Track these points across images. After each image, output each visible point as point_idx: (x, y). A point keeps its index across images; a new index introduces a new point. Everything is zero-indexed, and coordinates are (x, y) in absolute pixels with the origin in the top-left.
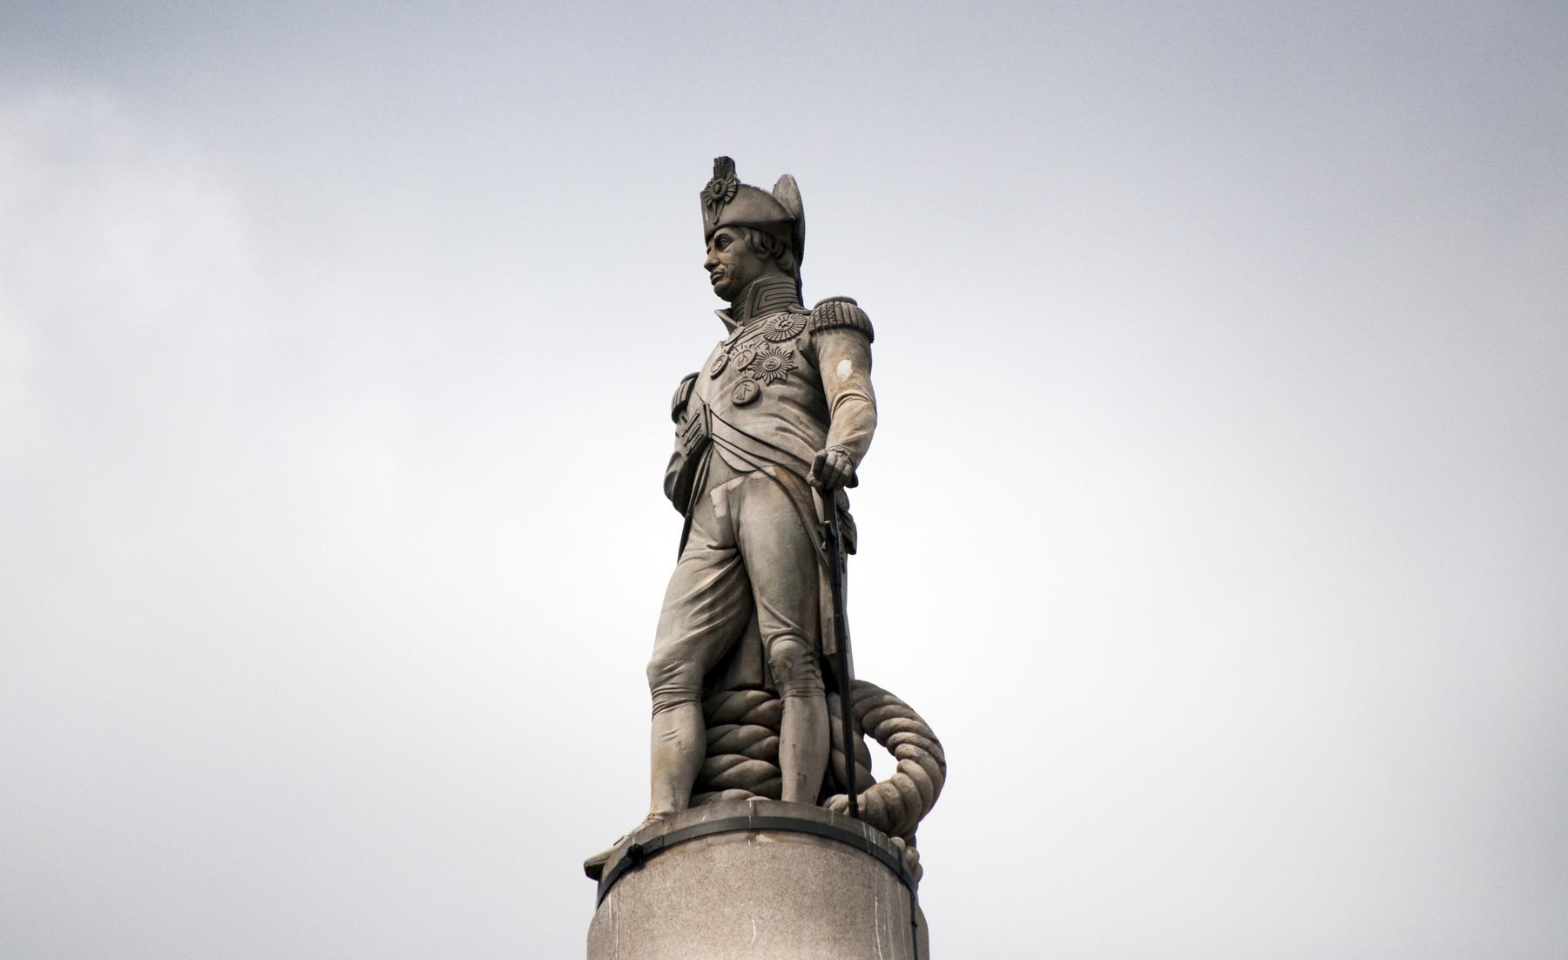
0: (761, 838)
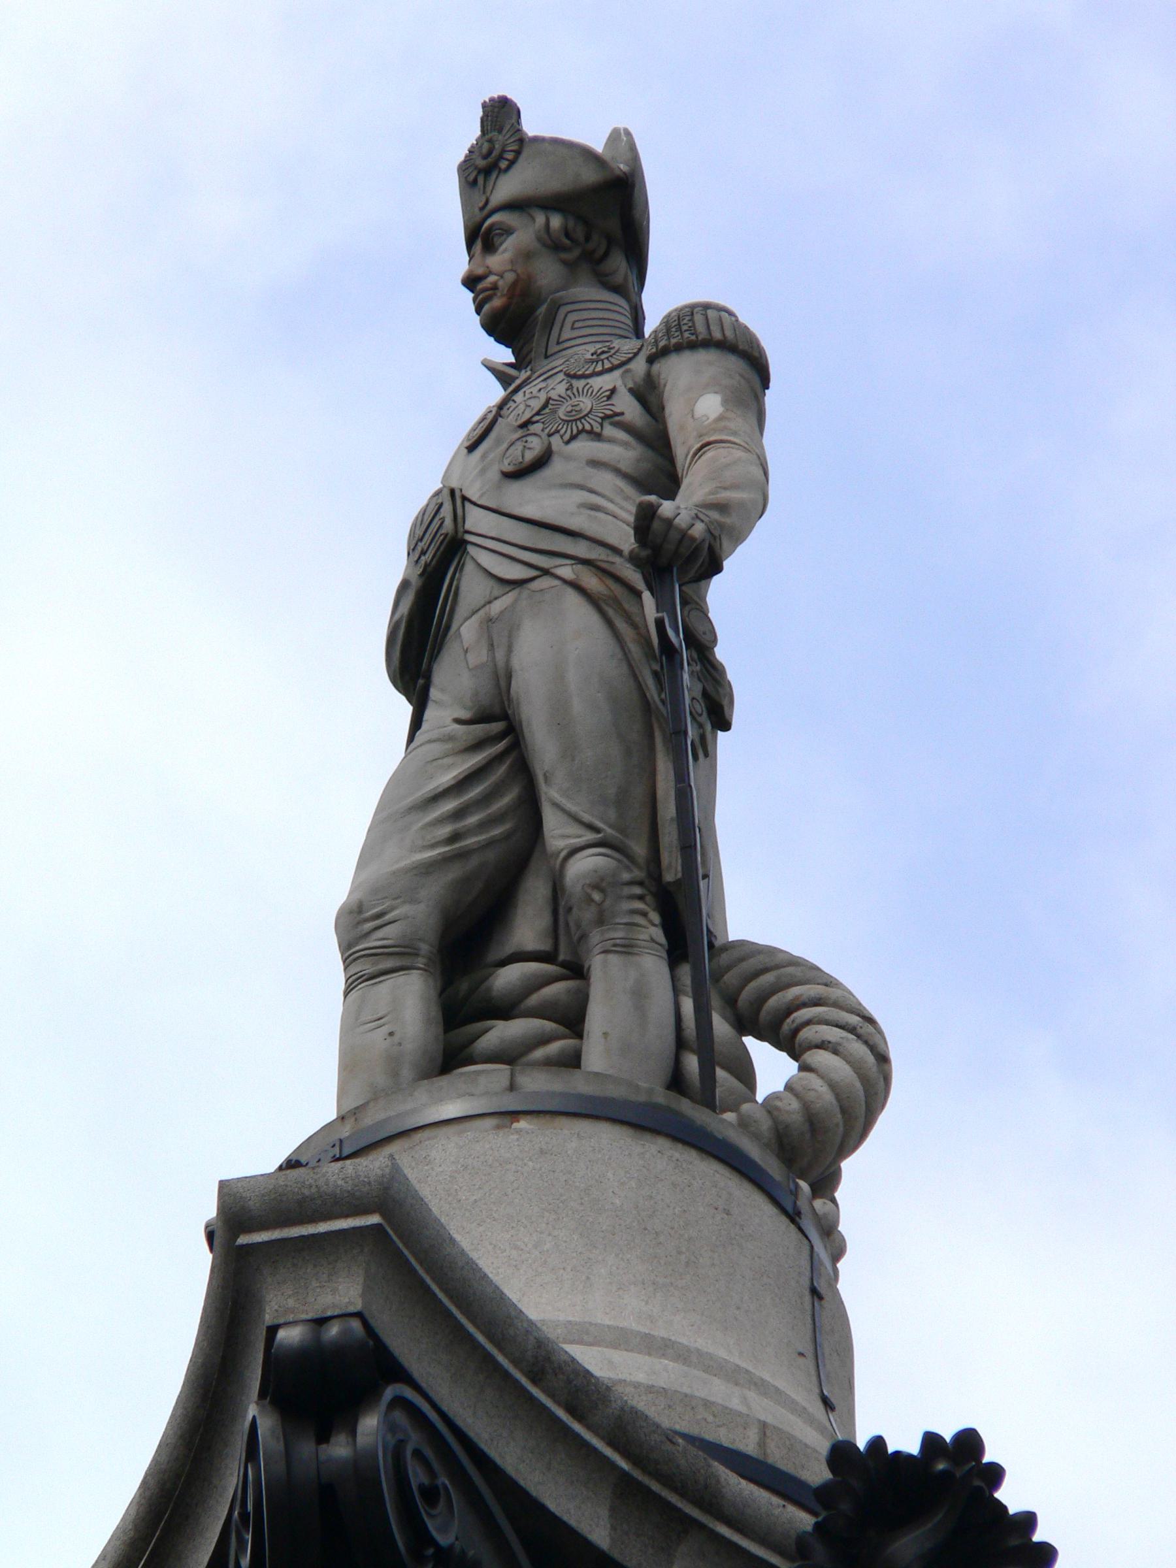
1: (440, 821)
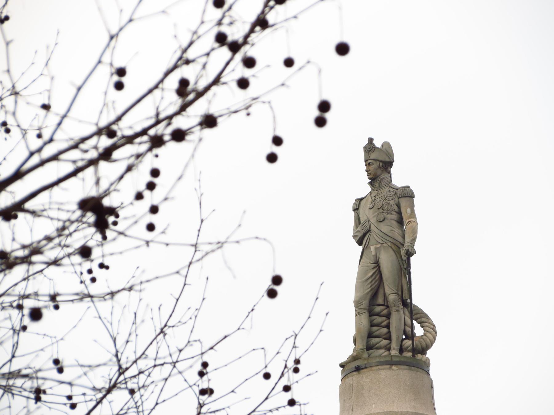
0: (394, 367)
1: (369, 284)
